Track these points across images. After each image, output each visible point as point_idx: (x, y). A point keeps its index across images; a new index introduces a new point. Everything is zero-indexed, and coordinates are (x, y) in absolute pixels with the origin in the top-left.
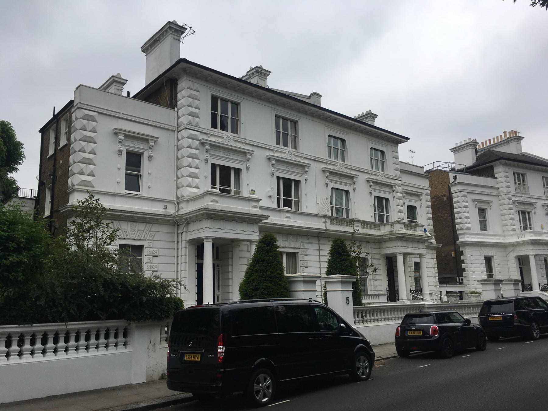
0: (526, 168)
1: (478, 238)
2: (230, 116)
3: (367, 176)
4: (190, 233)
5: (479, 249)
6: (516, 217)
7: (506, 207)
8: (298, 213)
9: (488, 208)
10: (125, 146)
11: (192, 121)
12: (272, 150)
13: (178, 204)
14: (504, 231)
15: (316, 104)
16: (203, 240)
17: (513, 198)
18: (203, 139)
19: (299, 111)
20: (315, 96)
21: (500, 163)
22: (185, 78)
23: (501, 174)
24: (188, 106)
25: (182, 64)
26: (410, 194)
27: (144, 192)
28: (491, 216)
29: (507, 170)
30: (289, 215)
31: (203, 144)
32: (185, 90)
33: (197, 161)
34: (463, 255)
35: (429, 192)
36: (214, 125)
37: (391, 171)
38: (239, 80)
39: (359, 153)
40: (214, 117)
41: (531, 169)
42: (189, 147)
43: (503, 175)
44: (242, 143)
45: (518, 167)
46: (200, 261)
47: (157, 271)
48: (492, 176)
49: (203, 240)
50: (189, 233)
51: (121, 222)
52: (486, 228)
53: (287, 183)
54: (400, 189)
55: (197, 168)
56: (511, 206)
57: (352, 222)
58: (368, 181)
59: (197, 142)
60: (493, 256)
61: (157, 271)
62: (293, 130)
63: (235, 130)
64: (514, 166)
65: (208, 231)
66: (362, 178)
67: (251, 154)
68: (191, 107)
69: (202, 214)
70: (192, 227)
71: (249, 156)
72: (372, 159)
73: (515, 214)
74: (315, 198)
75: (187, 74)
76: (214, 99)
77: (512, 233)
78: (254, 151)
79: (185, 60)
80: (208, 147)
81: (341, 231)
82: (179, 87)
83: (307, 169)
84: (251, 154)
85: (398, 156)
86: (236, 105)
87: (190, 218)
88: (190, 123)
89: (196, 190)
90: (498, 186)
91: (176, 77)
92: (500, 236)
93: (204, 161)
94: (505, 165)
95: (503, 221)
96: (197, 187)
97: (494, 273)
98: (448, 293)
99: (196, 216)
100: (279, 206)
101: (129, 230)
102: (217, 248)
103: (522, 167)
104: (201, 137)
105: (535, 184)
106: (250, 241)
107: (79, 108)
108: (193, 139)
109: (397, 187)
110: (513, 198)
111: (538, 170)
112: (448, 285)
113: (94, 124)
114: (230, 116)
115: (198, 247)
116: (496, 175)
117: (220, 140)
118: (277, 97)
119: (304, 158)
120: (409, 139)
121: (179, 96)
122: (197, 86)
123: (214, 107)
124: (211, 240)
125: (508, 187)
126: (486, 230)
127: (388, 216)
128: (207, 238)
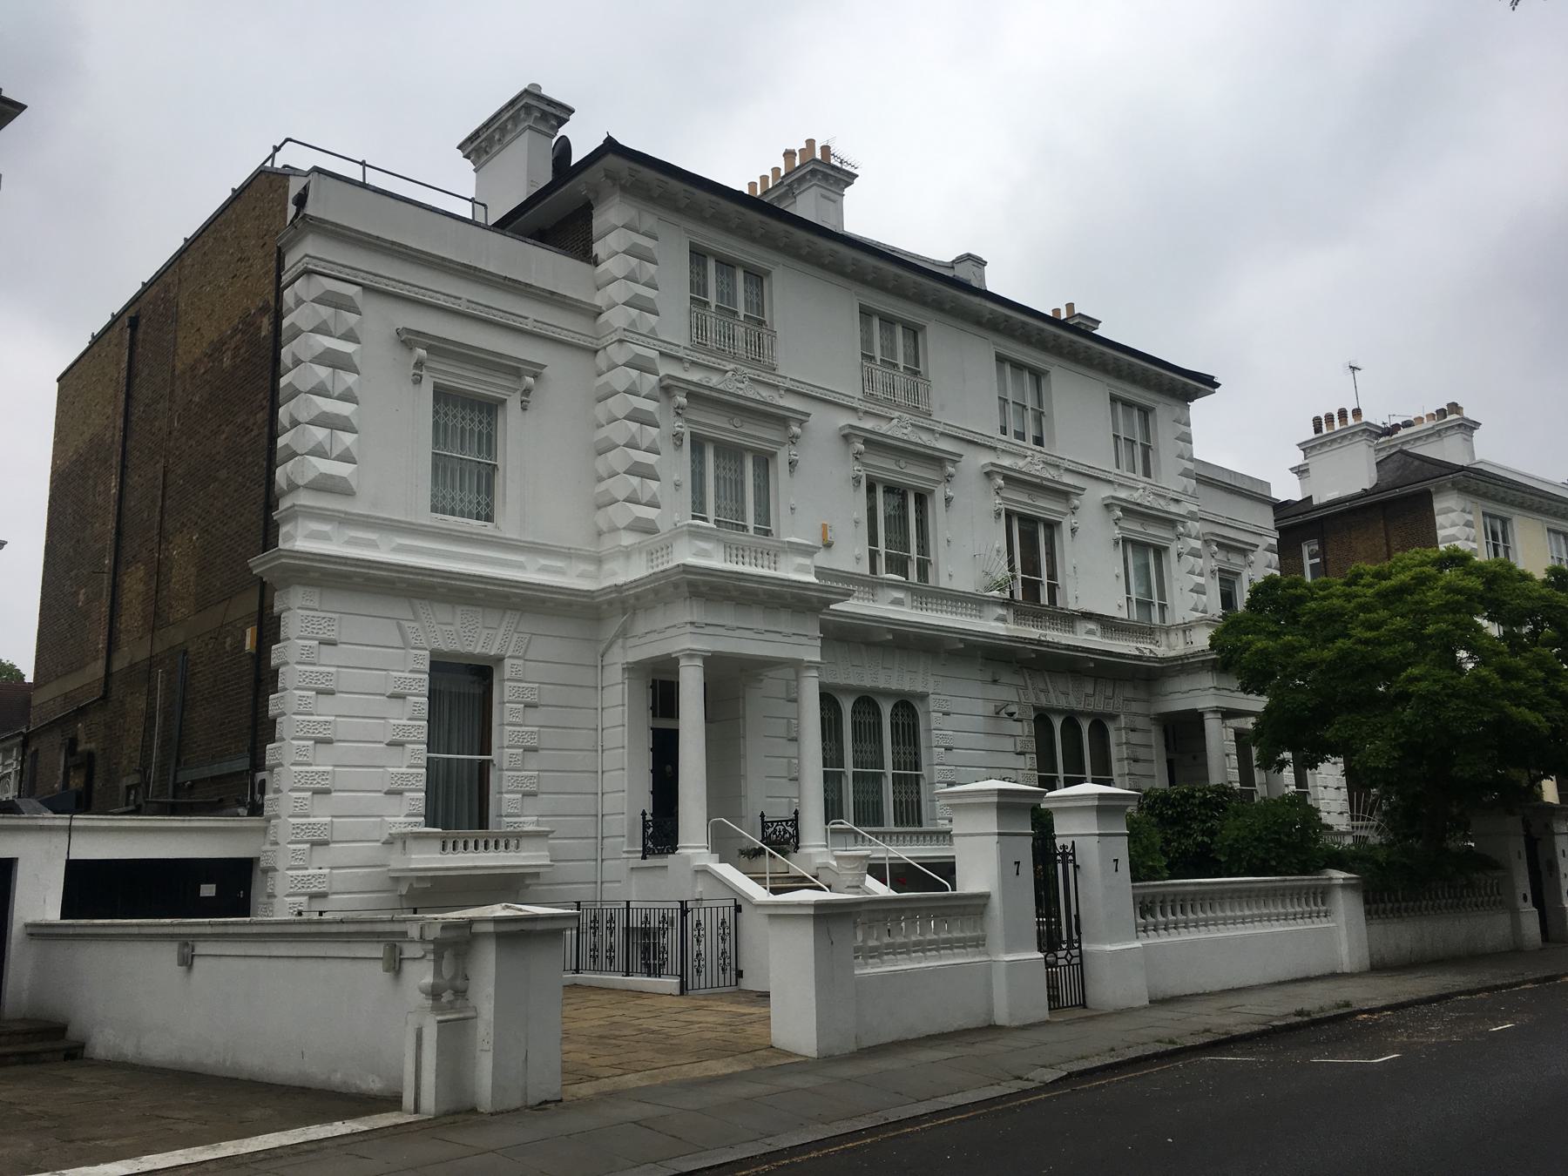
1: (544, 569)
3: (844, 420)
5: (400, 609)
6: (677, 466)
7: (619, 405)
8: (926, 594)
9: (513, 403)
10: (687, 421)
12: (855, 410)
14: (600, 534)
15: (975, 284)
17: (666, 369)
19: (920, 299)
20: (969, 263)
22: (616, 199)
25: (611, 160)
26: (1226, 547)
27: (507, 523)
28: (530, 447)
30: (899, 595)
32: (615, 227)
34: (278, 641)
35: (1274, 542)
37: (1169, 477)
38: (1053, 320)
39: (1081, 423)
42: (632, 391)
46: (665, 724)
48: (585, 254)
49: (677, 660)
50: (631, 642)
51: (416, 602)
52: (490, 505)
53: (1029, 525)
54: (1195, 527)
56: (650, 406)
57: (1071, 619)
58: (988, 474)
60: (500, 660)
62: (911, 351)
65: (686, 637)
66: (1096, 493)
67: (801, 423)
70: (641, 626)
71: (795, 429)
72: (1116, 437)
73: (667, 447)
74: (968, 546)
75: (624, 189)
76: (698, 255)
77: (628, 539)
78: (808, 415)
79: (611, 146)
80: (681, 400)
81: (1110, 653)
82: (598, 224)
83: (950, 469)
84: (801, 423)
85: (1190, 435)
90: (599, 300)
91: (591, 196)
92: (568, 554)
93: (851, 482)
95: (600, 479)
97: (924, 771)
98: (75, 870)
100: (873, 569)
106: (798, 666)
107: (308, 272)
109: (1189, 523)
110: (666, 369)
112: (80, 821)
113: (352, 318)
116: (598, 248)
118: (870, 261)
122: (649, 221)
123: (698, 286)
124: (699, 662)
126: (489, 518)
127: (1162, 607)
128: (691, 655)
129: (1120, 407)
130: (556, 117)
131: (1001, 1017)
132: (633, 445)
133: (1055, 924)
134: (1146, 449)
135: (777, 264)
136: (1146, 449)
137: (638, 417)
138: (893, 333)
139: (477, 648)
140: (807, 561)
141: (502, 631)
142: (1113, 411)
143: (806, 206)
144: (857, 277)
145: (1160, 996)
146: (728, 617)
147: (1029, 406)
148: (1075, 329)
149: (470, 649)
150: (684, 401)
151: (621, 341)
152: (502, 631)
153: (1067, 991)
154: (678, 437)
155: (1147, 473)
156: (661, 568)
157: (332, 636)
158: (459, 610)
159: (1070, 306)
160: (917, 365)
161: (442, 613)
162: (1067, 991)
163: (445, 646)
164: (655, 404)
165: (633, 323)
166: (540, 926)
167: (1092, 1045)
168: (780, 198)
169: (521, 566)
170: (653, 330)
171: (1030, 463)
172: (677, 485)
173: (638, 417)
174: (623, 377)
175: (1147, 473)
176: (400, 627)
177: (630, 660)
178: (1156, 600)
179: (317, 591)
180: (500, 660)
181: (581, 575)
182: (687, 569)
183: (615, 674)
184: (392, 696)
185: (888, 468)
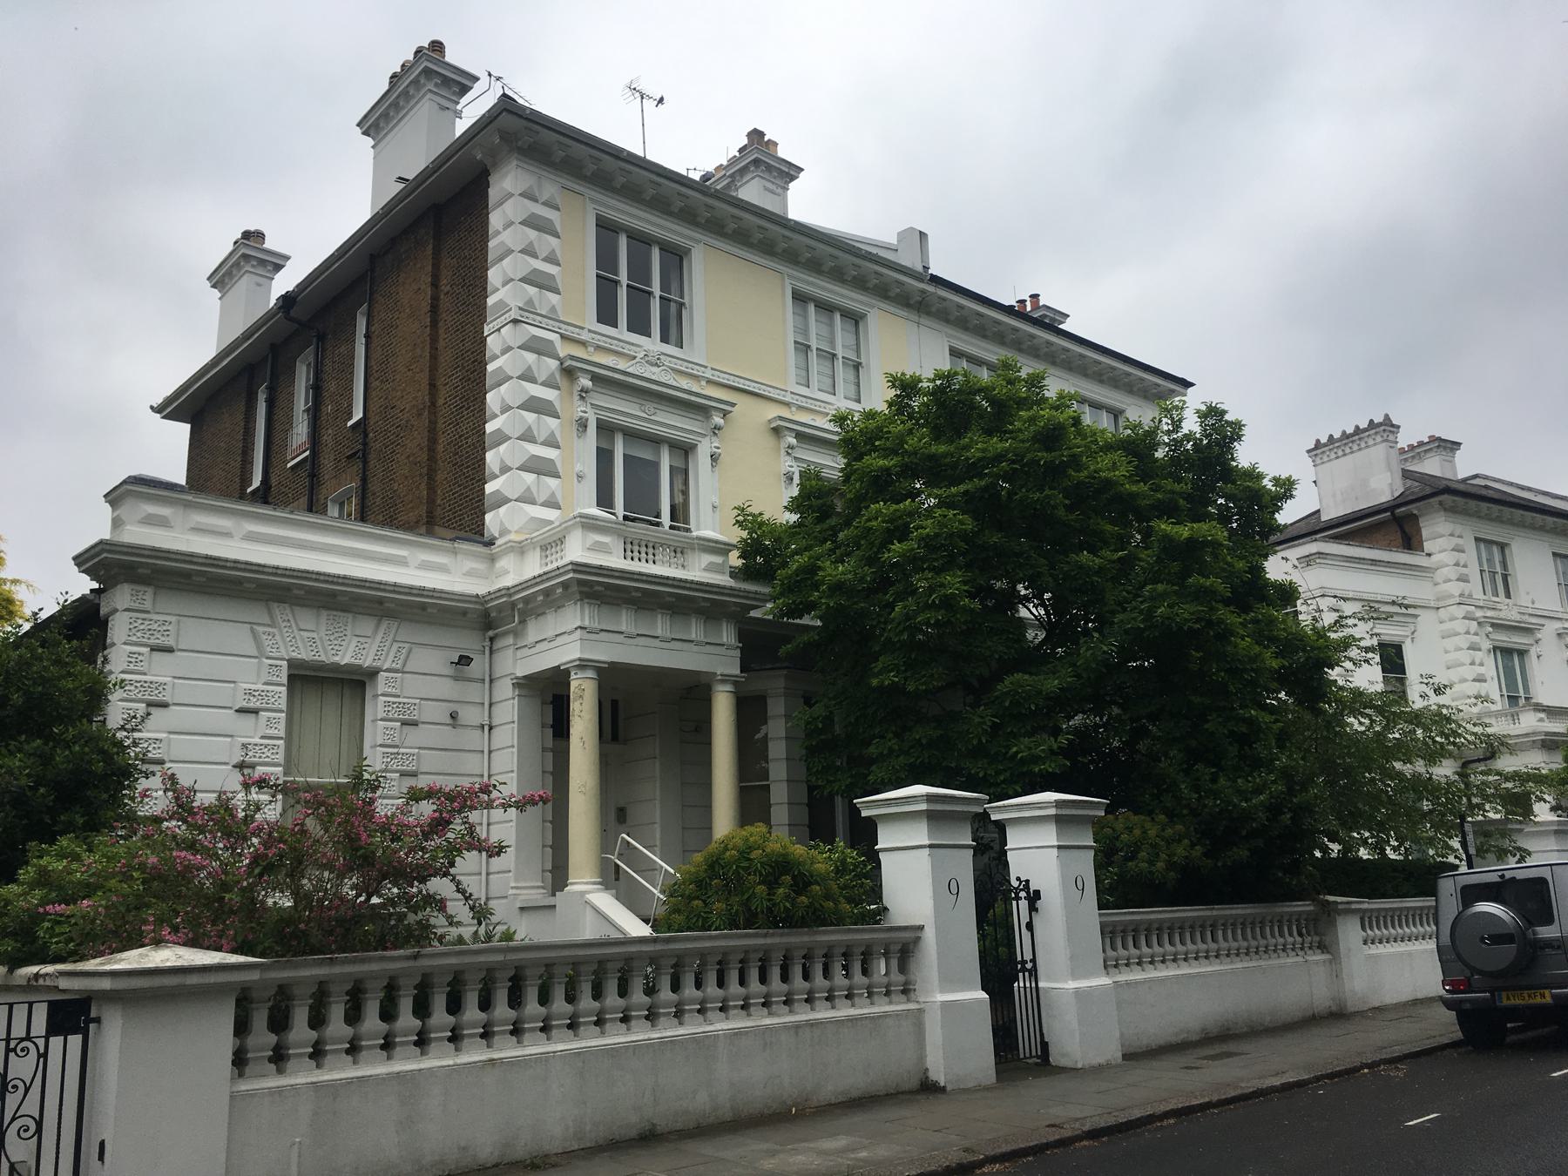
0: (1511, 523)
2: (656, 288)
3: (773, 412)
4: (526, 652)
5: (257, 613)
11: (534, 368)
13: (491, 728)
16: (567, 673)
17: (563, 350)
18: (572, 358)
21: (1441, 503)
23: (1442, 542)
24: (522, 377)
29: (1458, 529)
31: (569, 373)
33: (553, 423)
36: (606, 314)
38: (1009, 310)
40: (606, 288)
41: (1522, 525)
42: (528, 376)
43: (1445, 541)
44: (696, 378)
45: (1489, 518)
47: (414, 775)
49: (567, 673)
50: (520, 654)
51: (297, 610)
55: (552, 443)
56: (549, 394)
58: (777, 431)
59: (553, 364)
60: (373, 673)
61: (414, 775)
63: (672, 331)
64: (1477, 515)
66: (752, 416)
67: (725, 414)
68: (533, 502)
69: (565, 585)
70: (534, 631)
76: (607, 229)
78: (733, 405)
80: (586, 382)
82: (494, 193)
86: (676, 258)
87: (526, 600)
88: (528, 308)
89: (551, 514)
93: (575, 427)
94: (1452, 511)
96: (552, 504)
99: (547, 593)
101: (323, 634)
102: (615, 703)
103: (1499, 520)
104: (1479, 613)
105: (1535, 570)
108: (541, 287)
111: (1542, 529)
114: (656, 288)
115: (549, 694)
117: (622, 365)
119: (709, 382)
120: (1192, 385)
121: (495, 220)
122: (550, 188)
123: (606, 260)
124: (591, 674)
125: (1463, 579)
129: (1482, 546)
130: (459, 83)
131: (938, 1075)
132: (527, 437)
133: (1002, 967)
134: (1505, 578)
135: (697, 241)
136: (1505, 578)
137: (533, 405)
138: (805, 311)
139: (345, 658)
140: (718, 559)
141: (379, 638)
142: (1478, 549)
143: (752, 192)
144: (791, 257)
145: (1132, 1050)
146: (626, 621)
147: (840, 352)
148: (1037, 322)
149: (336, 659)
150: (589, 384)
151: (515, 321)
152: (379, 638)
153: (1017, 1045)
154: (582, 425)
155: (1508, 596)
156: (554, 565)
157: (169, 641)
158: (324, 613)
159: (1035, 297)
160: (859, 356)
161: (307, 618)
162: (1017, 1045)
163: (304, 654)
164: (556, 392)
165: (530, 302)
166: (193, 980)
167: (1038, 1111)
168: (728, 186)
169: (402, 562)
170: (553, 309)
171: (1509, 613)
172: (580, 477)
173: (533, 405)
174: (1460, 626)
175: (1508, 596)
176: (252, 630)
177: (520, 674)
178: (1522, 693)
179: (150, 590)
180: (373, 673)
181: (469, 574)
182: (578, 567)
183: (505, 690)
184: (240, 711)
185: (1505, 639)
